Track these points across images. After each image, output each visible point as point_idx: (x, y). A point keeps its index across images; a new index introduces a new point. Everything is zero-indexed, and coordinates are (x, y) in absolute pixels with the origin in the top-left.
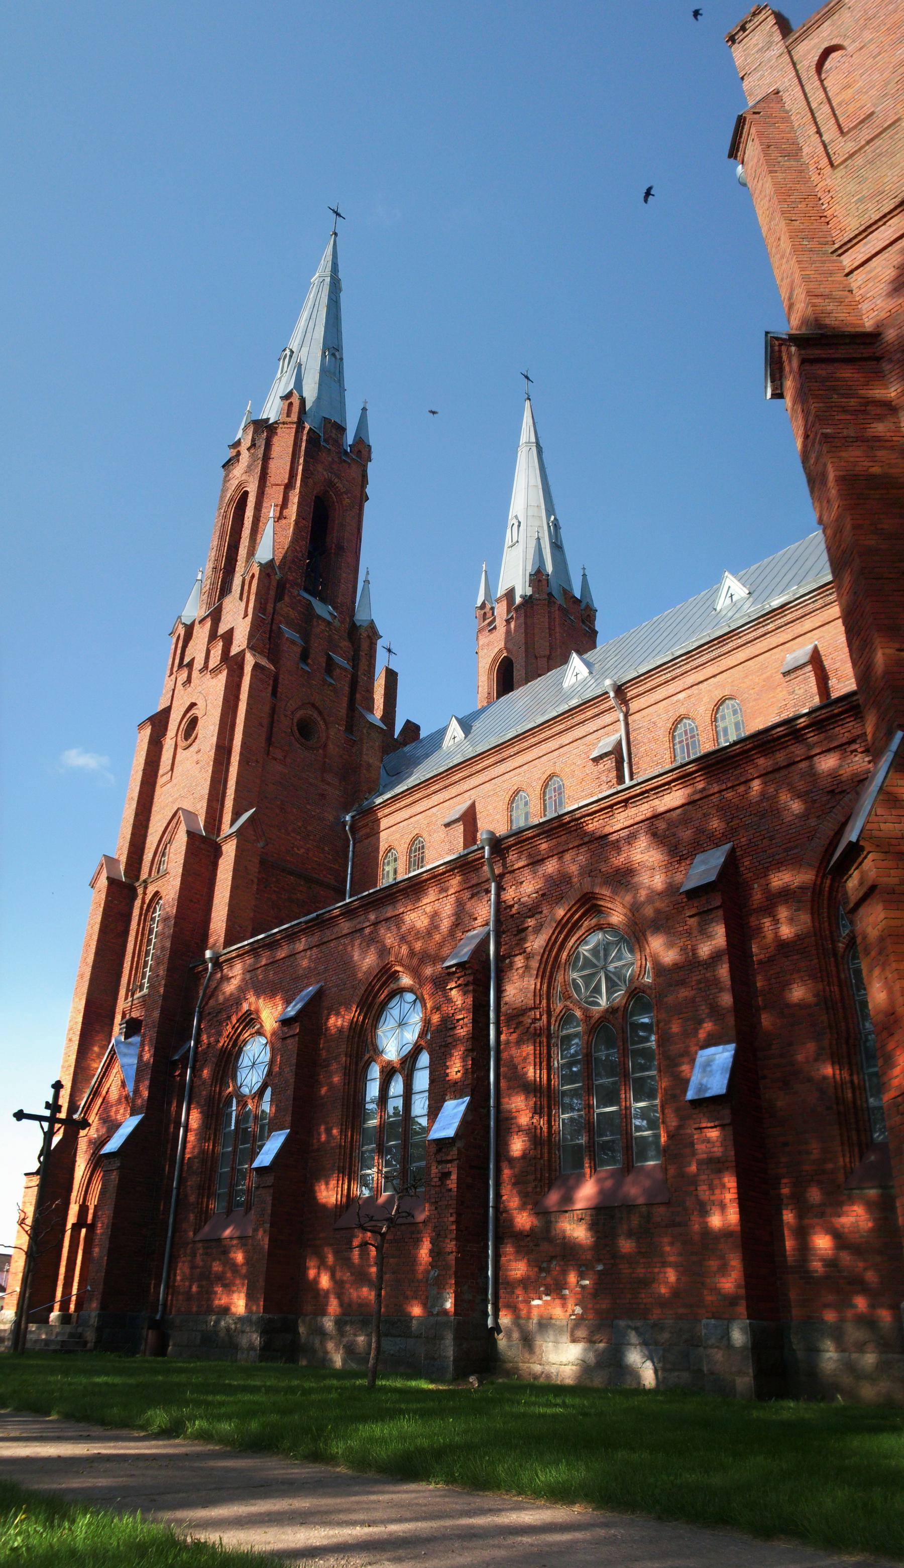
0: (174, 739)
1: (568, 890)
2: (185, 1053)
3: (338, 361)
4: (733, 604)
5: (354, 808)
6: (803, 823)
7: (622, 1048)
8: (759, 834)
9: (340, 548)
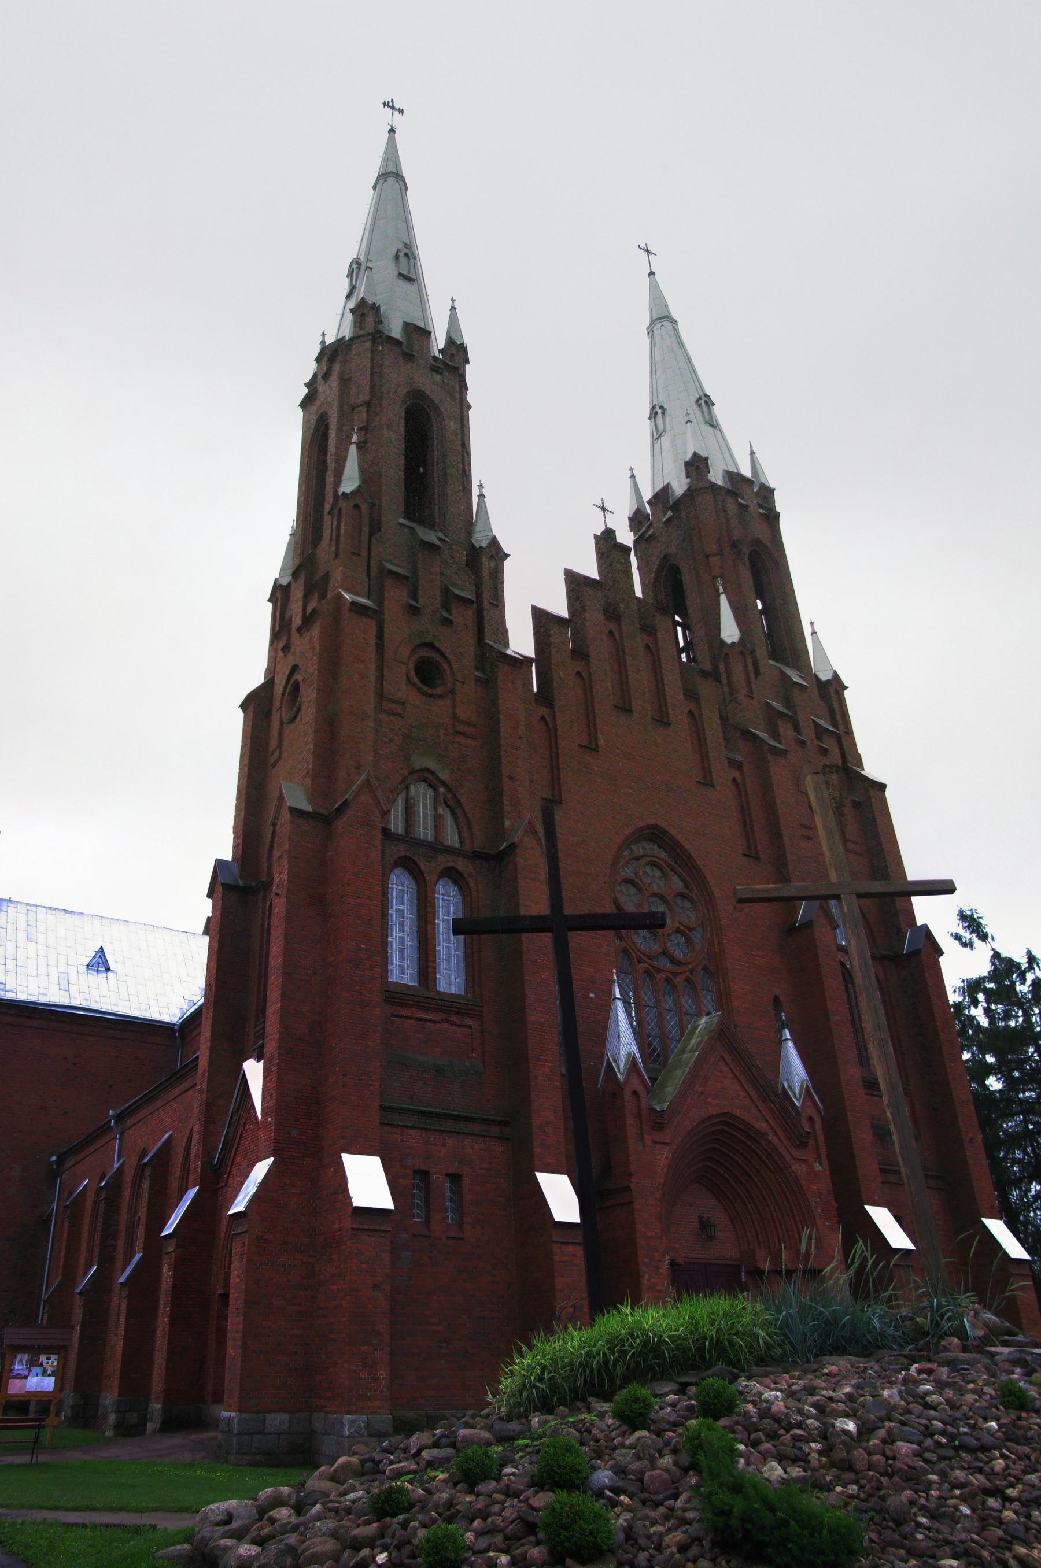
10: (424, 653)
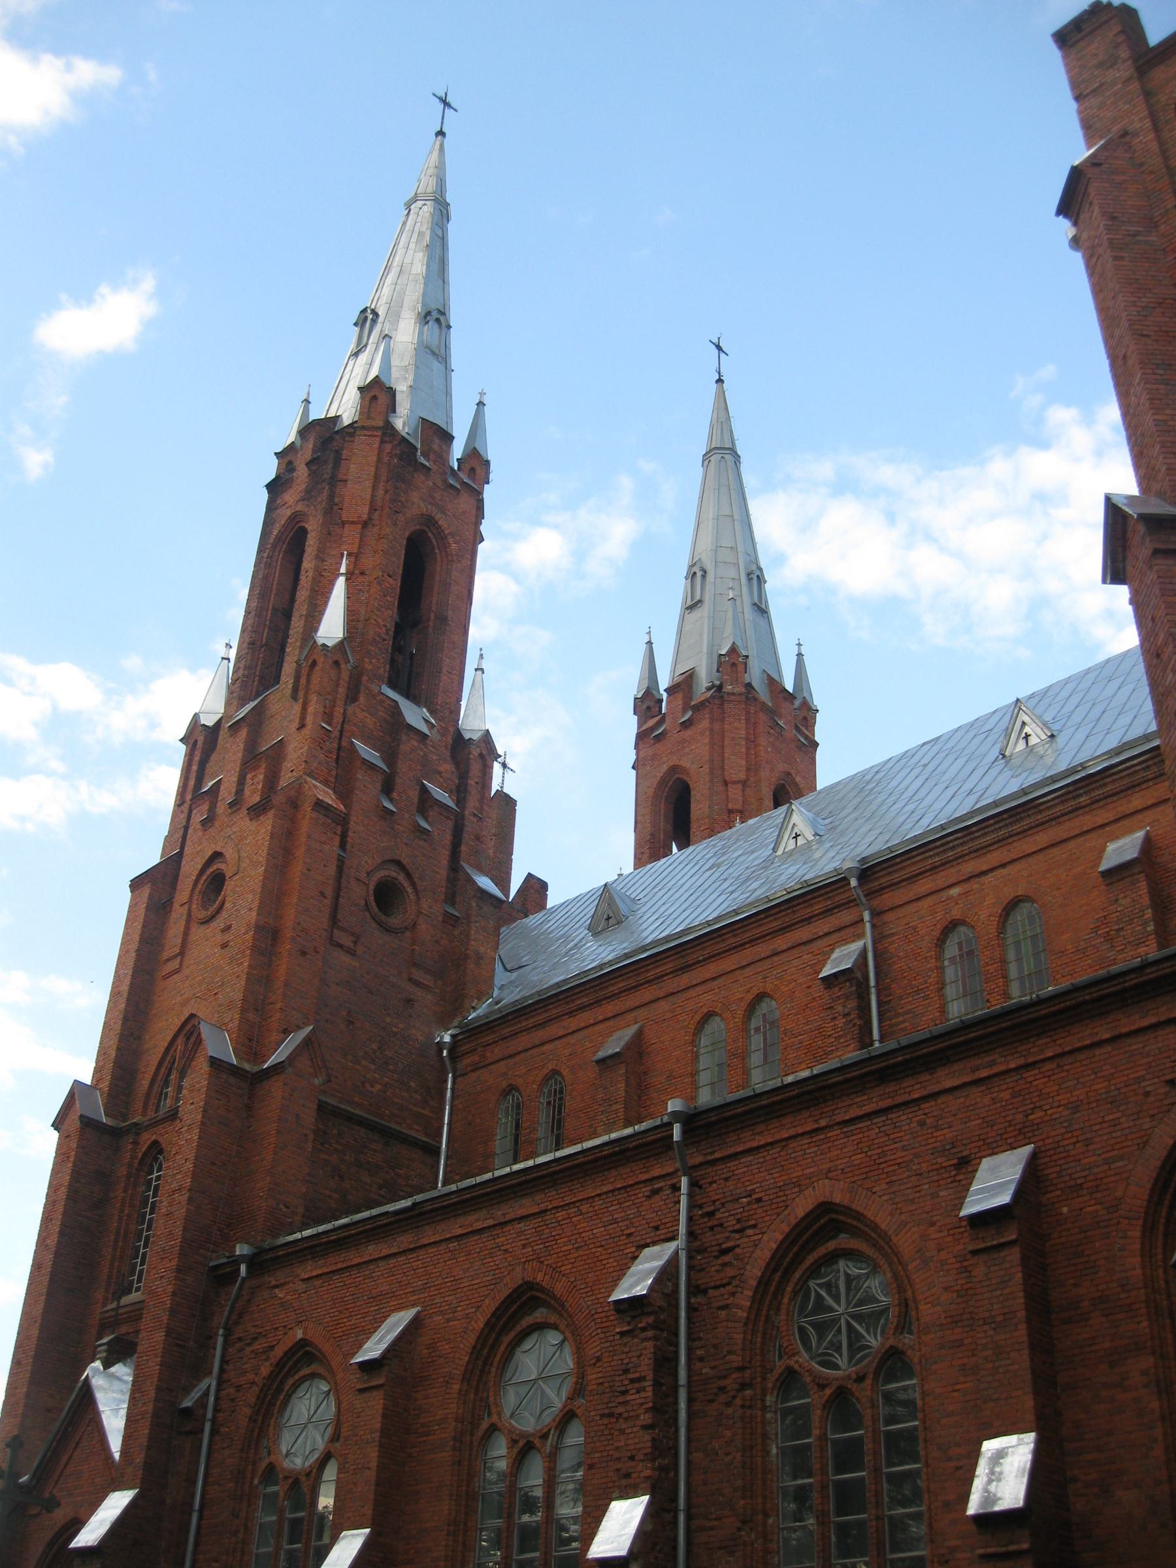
0: (186, 907)
1: (794, 1196)
2: (201, 1397)
3: (444, 329)
4: (1029, 750)
5: (456, 1023)
6: (1132, 1124)
7: (870, 1429)
8: (1070, 1135)
9: (442, 619)
10: (393, 872)
